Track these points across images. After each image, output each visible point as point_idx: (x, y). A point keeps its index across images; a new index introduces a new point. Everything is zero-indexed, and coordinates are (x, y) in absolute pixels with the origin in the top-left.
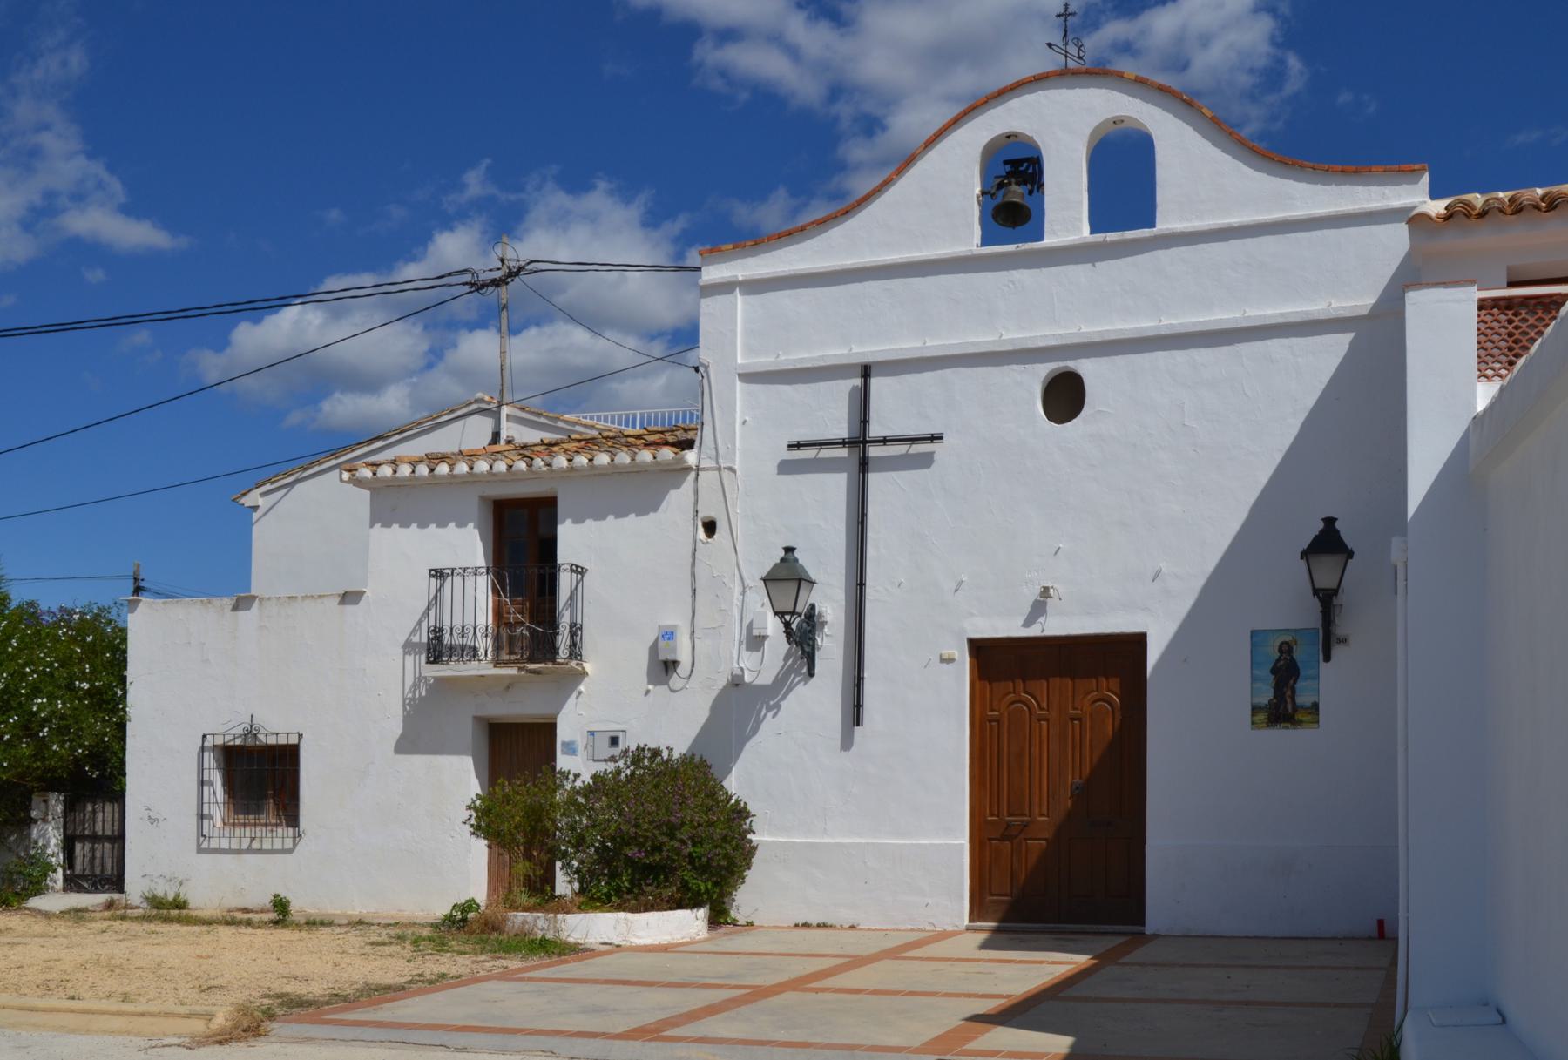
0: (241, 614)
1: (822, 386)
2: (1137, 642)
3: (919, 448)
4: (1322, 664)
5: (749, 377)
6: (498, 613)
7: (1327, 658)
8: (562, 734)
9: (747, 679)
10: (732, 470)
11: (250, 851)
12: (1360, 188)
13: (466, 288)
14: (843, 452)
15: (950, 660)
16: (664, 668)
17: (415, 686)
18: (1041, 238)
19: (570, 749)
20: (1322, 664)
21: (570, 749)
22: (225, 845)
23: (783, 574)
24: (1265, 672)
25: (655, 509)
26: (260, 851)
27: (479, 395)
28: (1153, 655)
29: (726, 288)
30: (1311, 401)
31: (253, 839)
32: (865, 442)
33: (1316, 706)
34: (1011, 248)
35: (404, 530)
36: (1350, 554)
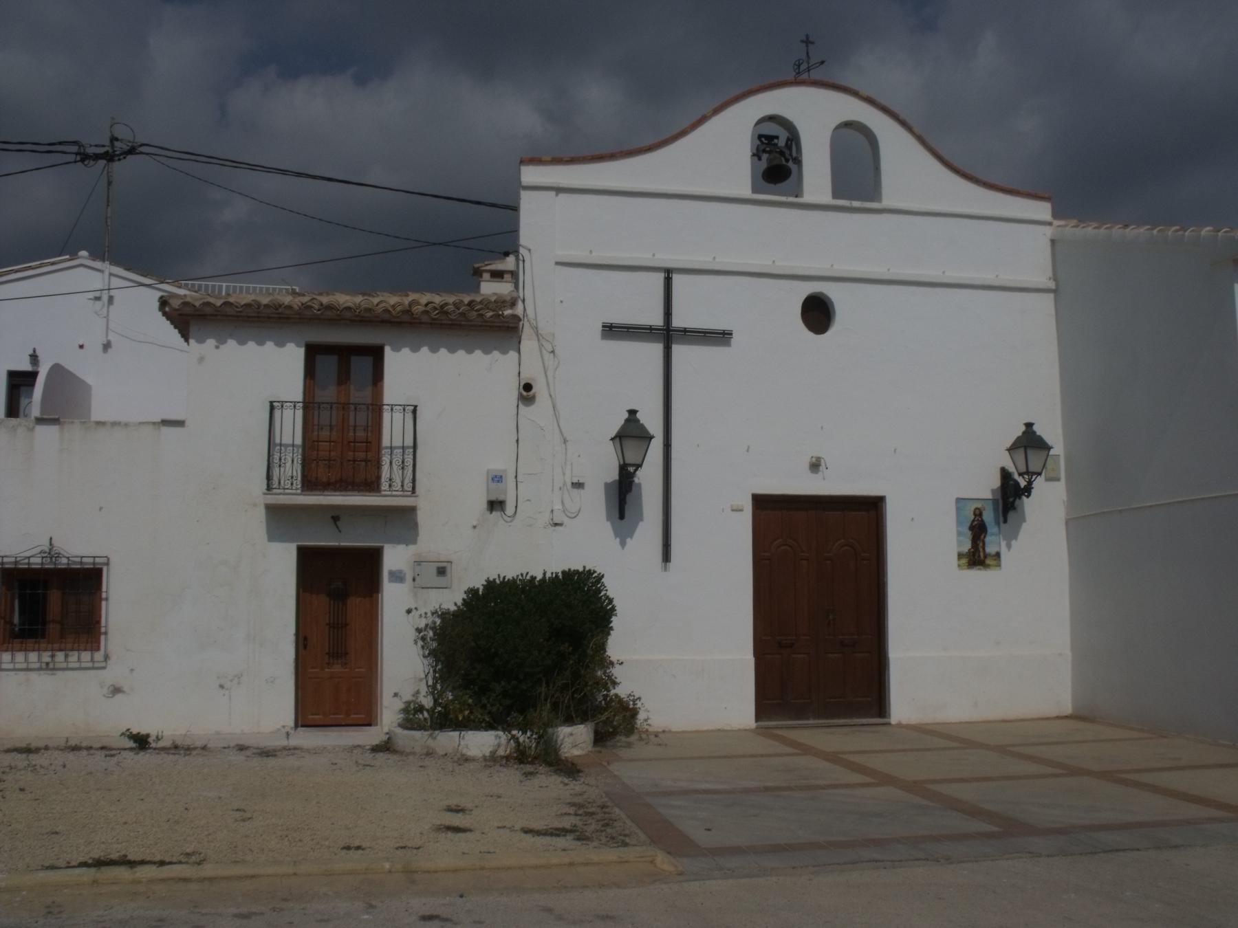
13: (72, 158)
33: (998, 555)
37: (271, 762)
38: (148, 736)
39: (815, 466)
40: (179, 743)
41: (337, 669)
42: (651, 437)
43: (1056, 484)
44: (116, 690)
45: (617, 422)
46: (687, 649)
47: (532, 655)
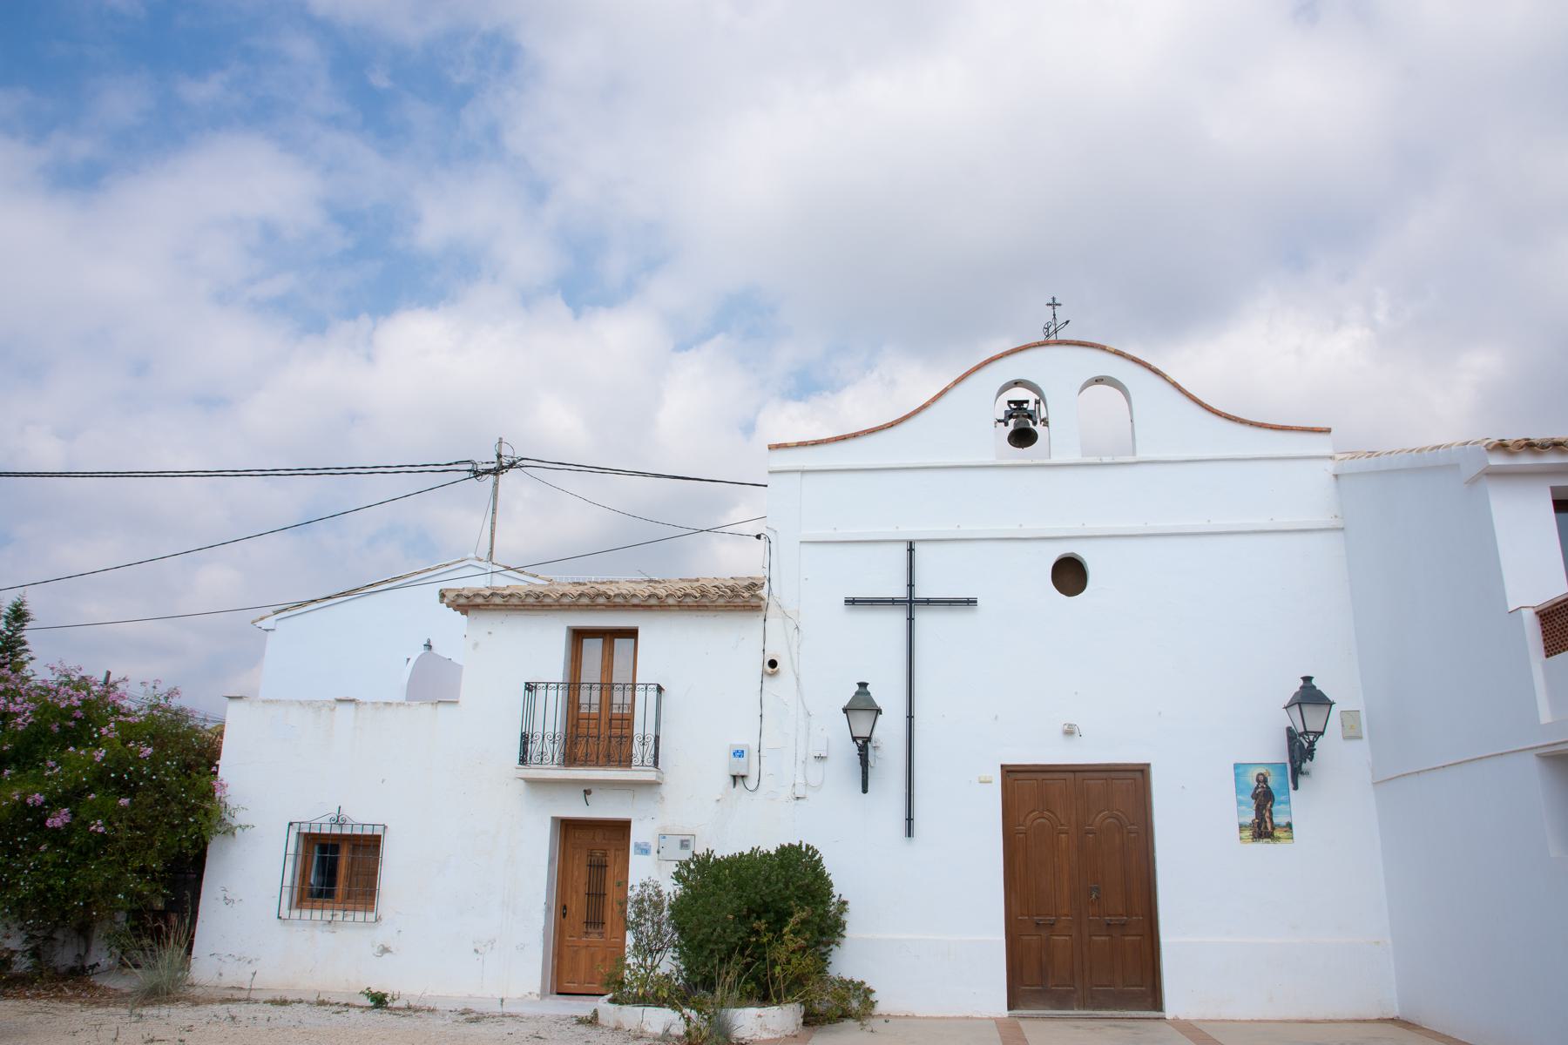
7: (1296, 788)
8: (637, 835)
13: (467, 474)
23: (863, 705)
32: (911, 601)
33: (1289, 826)
36: (1331, 704)
37: (474, 1028)
38: (385, 995)
39: (1069, 732)
40: (412, 1003)
41: (594, 938)
43: (1357, 742)
44: (385, 950)
45: (848, 693)
46: (927, 919)
47: (765, 923)
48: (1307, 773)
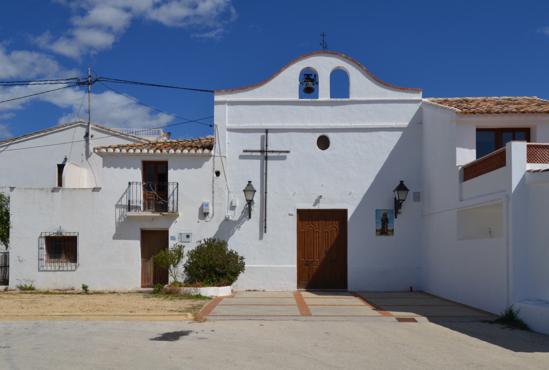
0: (55, 193)
1: (252, 134)
2: (345, 212)
3: (282, 155)
4: (395, 219)
5: (230, 130)
6: (145, 196)
7: (396, 218)
8: (171, 234)
9: (230, 219)
10: (225, 157)
11: (59, 270)
12: (405, 93)
14: (259, 154)
15: (292, 215)
16: (204, 214)
17: (120, 218)
18: (318, 98)
19: (173, 238)
20: (395, 219)
21: (173, 238)
22: (49, 269)
23: (250, 189)
24: (379, 221)
25: (201, 167)
26: (63, 271)
27: (81, 120)
28: (349, 215)
29: (223, 103)
30: (391, 149)
31: (60, 267)
33: (393, 230)
34: (310, 100)
35: (115, 169)
36: (408, 190)
42: (255, 191)
45: (244, 185)
48: (400, 213)
